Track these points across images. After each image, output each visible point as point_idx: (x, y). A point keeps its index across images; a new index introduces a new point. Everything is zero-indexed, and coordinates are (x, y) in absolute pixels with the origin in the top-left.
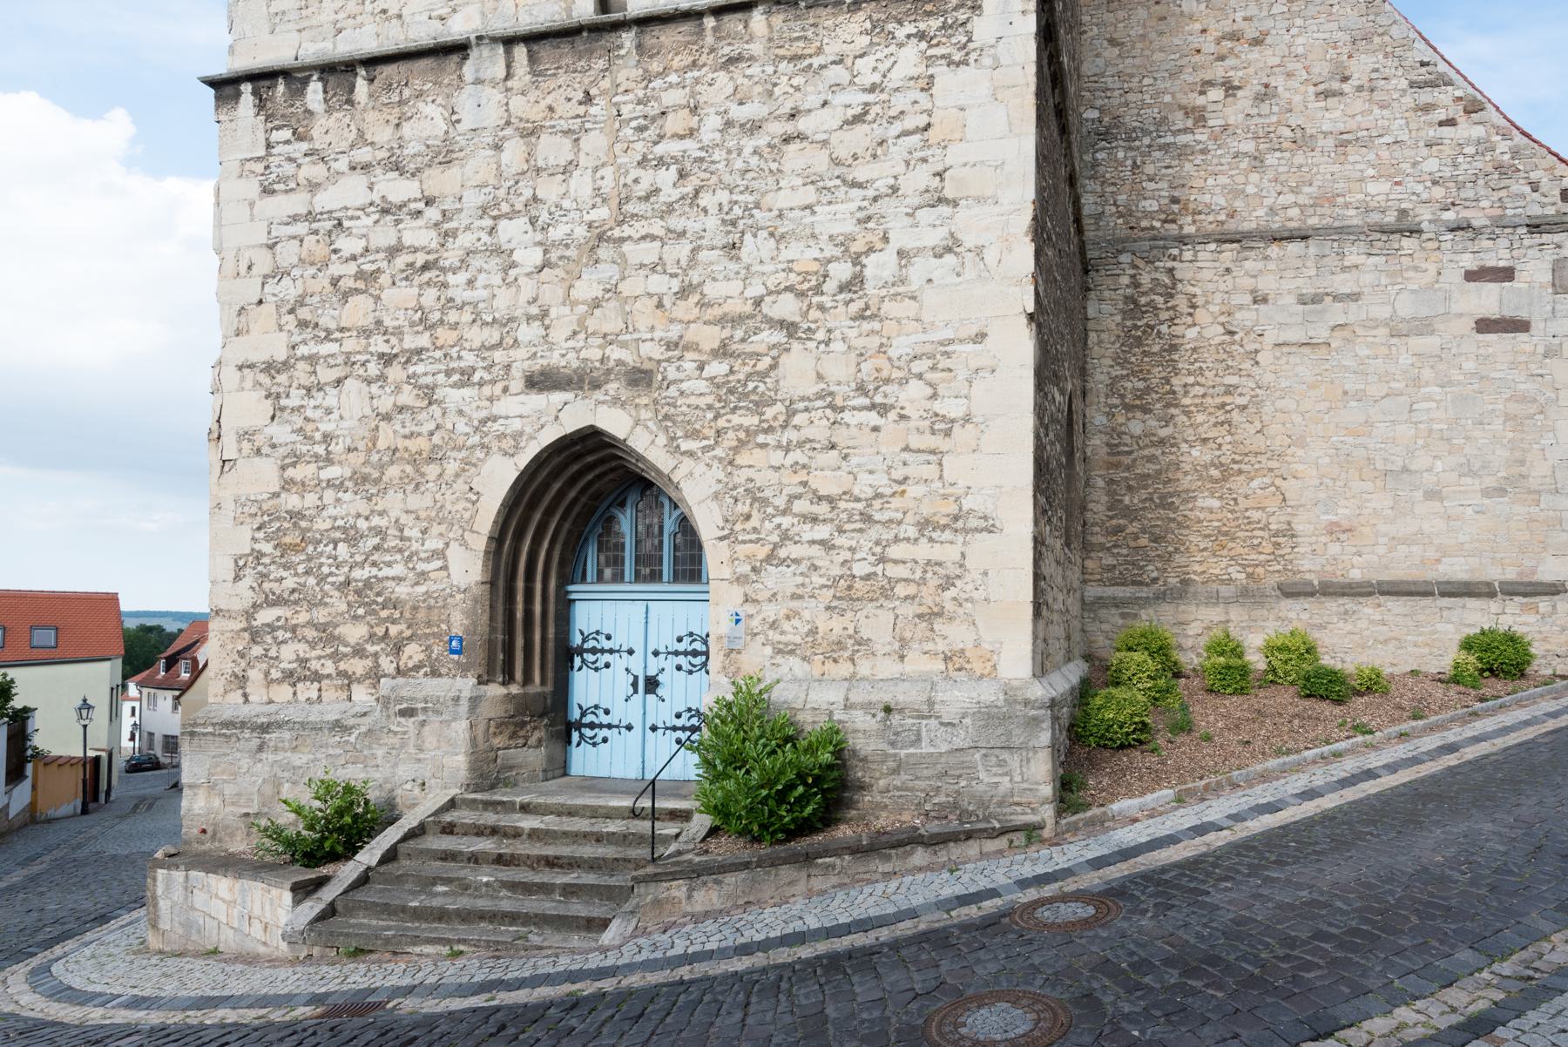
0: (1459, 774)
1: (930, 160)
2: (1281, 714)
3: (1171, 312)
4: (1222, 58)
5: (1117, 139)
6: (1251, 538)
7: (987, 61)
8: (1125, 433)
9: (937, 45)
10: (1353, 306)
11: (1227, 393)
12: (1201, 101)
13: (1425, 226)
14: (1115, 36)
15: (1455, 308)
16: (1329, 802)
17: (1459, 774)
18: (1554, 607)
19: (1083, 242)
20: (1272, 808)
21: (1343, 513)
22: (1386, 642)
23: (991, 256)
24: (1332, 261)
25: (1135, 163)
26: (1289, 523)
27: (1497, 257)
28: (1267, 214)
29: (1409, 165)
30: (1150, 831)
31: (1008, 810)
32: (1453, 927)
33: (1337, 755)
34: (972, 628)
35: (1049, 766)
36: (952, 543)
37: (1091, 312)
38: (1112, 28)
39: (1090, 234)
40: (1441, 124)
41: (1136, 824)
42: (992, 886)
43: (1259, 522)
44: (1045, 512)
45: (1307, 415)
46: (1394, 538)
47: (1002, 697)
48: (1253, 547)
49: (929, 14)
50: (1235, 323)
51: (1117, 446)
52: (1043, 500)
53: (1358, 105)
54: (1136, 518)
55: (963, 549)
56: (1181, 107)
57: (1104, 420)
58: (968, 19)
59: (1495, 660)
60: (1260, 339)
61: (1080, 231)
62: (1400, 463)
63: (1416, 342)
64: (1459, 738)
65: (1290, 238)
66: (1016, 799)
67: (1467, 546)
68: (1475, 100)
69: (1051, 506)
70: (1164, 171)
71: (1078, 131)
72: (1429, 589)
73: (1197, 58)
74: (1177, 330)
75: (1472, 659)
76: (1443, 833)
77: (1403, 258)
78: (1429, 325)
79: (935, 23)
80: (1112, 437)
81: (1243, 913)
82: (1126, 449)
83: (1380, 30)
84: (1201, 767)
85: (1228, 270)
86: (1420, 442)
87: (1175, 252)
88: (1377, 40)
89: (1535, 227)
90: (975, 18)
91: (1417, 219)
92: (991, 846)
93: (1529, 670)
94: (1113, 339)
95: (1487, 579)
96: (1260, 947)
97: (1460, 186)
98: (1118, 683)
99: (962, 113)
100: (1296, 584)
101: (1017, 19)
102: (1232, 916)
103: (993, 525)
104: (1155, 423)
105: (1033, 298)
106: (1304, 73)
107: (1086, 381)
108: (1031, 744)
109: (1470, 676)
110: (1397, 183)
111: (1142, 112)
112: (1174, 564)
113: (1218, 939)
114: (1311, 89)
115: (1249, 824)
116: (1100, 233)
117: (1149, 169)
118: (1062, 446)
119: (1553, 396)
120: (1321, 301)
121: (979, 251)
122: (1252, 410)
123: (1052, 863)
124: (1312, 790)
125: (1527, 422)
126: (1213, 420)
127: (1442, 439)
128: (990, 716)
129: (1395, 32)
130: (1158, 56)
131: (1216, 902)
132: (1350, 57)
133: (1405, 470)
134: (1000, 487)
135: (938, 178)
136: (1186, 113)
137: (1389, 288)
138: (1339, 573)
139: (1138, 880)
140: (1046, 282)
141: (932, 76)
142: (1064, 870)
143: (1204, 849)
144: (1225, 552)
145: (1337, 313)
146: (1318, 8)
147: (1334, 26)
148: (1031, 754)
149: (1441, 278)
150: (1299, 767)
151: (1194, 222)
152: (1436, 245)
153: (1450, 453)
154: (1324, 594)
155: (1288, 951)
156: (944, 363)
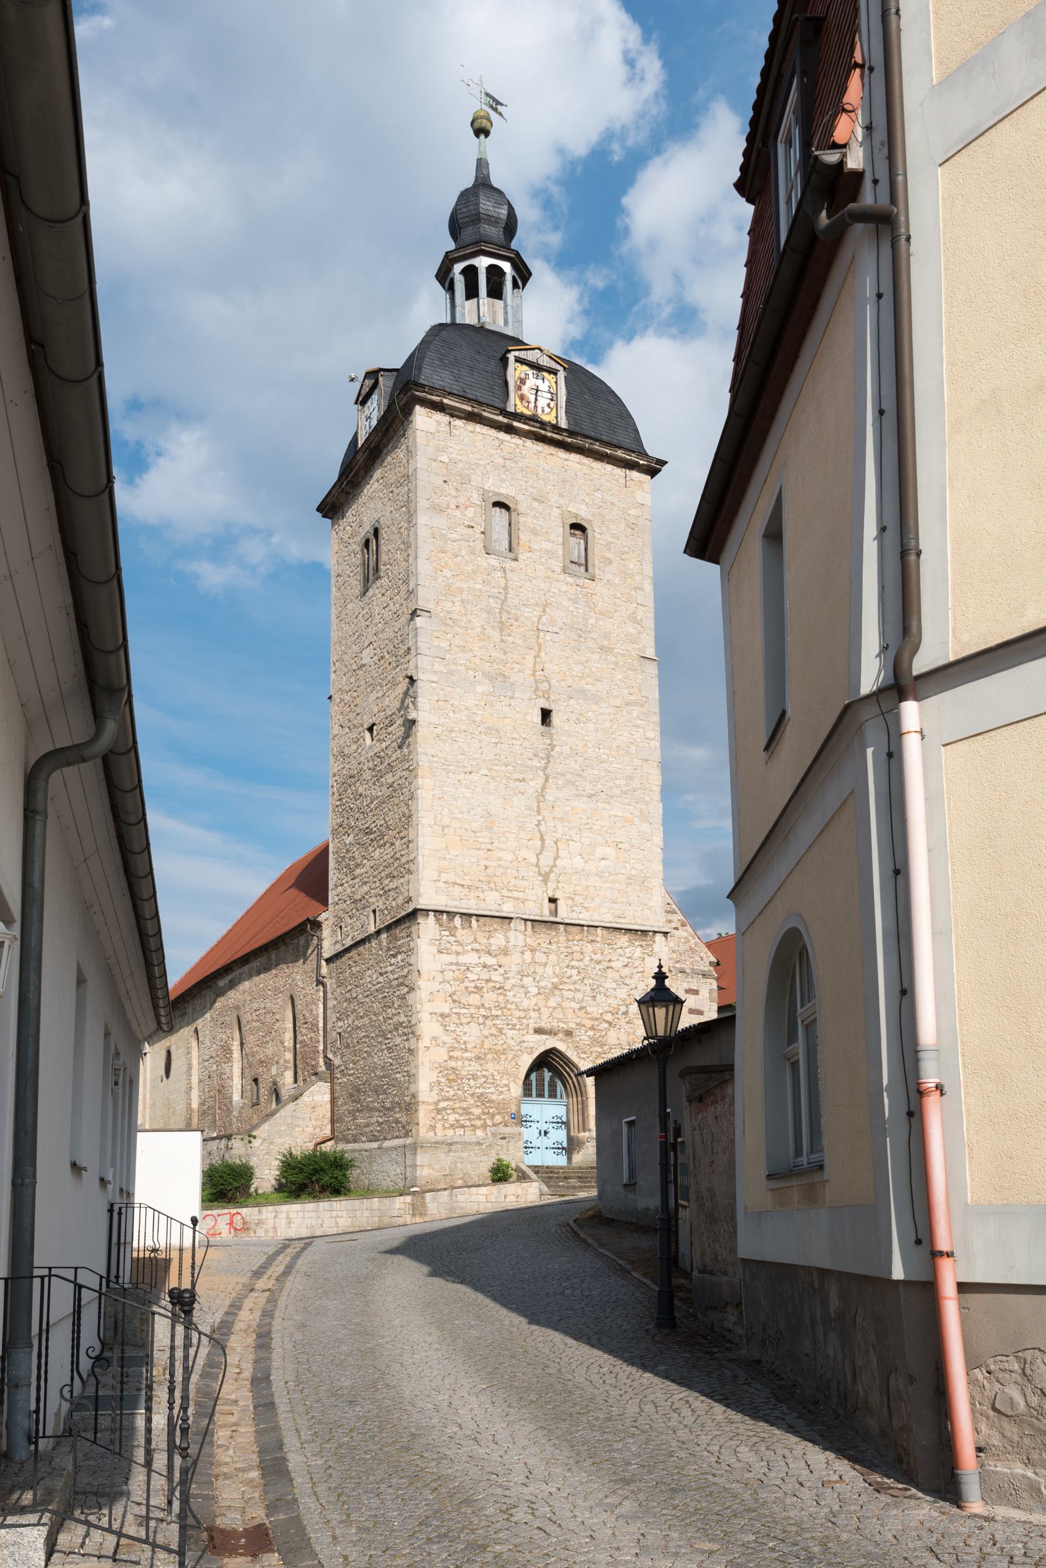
97: (681, 954)
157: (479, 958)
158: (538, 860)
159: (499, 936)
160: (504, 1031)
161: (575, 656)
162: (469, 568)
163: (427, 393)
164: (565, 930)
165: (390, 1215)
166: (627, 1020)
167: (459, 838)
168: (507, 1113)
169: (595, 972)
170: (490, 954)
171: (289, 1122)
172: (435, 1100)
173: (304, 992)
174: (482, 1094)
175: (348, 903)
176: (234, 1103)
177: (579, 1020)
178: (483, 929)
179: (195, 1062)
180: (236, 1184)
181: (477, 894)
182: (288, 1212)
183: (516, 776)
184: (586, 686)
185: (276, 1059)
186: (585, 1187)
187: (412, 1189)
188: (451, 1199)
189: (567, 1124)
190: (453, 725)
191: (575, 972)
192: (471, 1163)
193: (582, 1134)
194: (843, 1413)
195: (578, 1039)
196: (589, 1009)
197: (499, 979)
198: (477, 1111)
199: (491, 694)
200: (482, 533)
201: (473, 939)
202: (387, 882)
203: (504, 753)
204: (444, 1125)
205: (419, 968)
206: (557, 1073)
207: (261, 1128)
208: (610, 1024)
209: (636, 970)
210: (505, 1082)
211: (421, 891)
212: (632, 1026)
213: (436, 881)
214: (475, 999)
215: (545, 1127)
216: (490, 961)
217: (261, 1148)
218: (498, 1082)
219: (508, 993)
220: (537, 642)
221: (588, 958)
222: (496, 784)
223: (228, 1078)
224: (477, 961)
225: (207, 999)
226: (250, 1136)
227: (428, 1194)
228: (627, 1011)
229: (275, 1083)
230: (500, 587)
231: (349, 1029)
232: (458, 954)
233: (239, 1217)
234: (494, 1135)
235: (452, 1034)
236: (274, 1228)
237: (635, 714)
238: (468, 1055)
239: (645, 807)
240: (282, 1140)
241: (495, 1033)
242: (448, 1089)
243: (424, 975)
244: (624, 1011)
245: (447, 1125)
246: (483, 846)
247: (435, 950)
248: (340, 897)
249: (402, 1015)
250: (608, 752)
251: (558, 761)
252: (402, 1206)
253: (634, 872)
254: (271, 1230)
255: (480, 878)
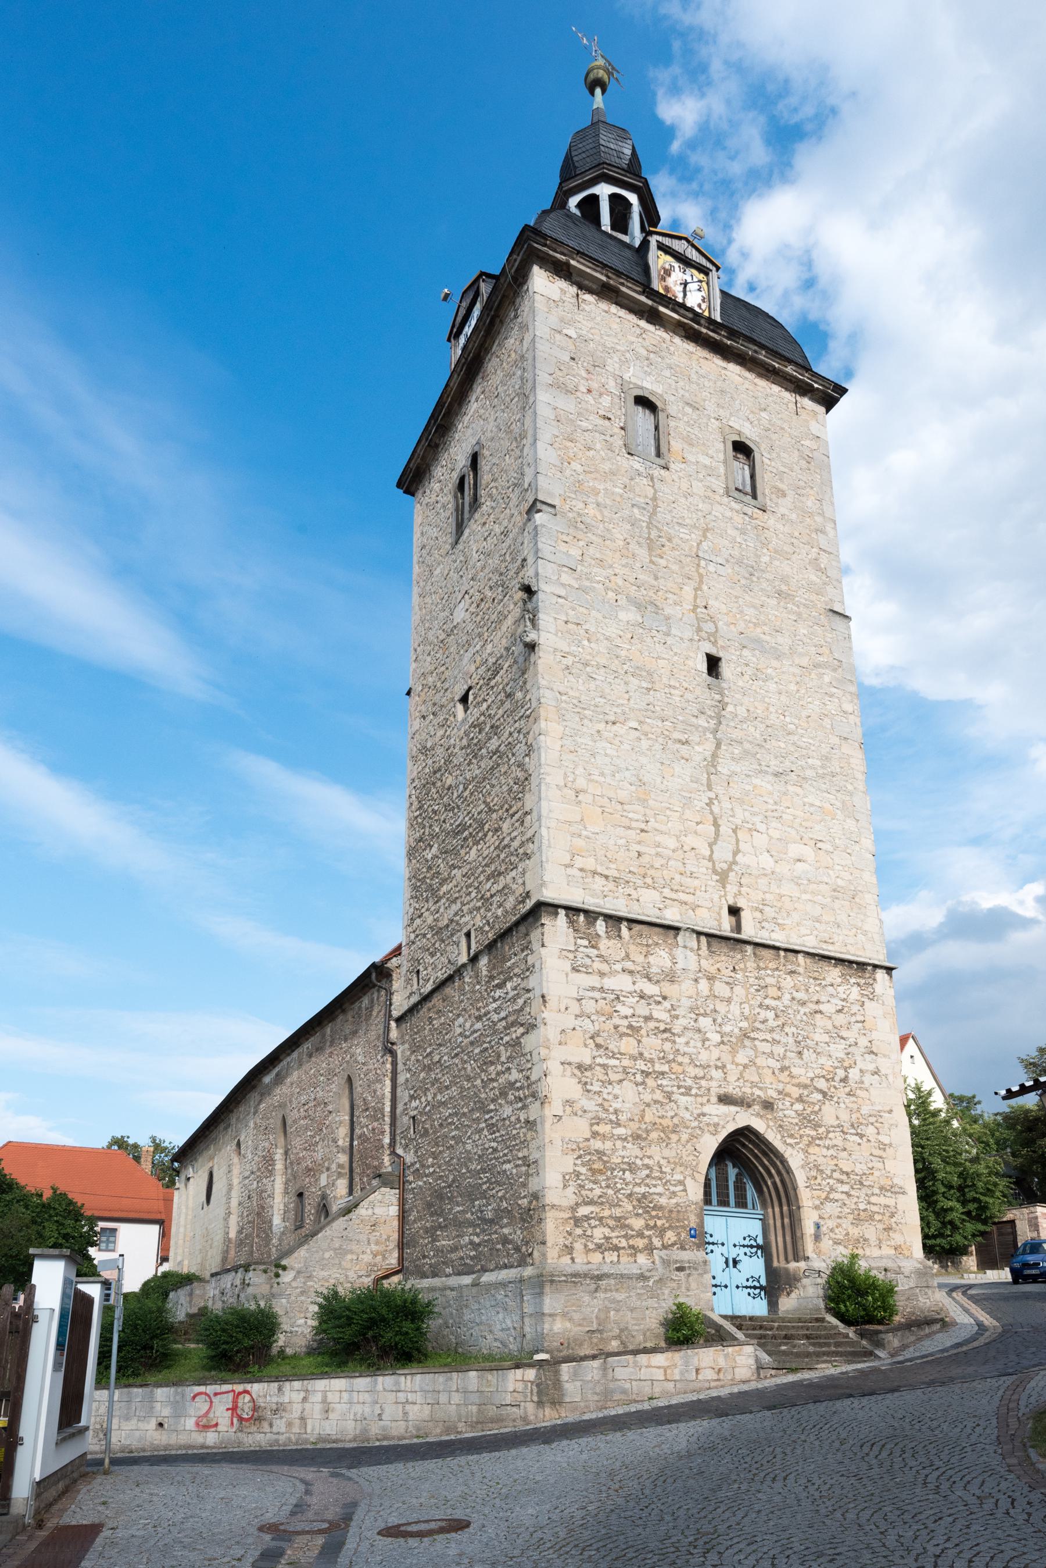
157: (634, 983)
158: (712, 852)
159: (662, 953)
160: (674, 1097)
161: (747, 597)
162: (607, 466)
163: (549, 247)
164: (754, 954)
165: (498, 1402)
166: (847, 1089)
167: (600, 810)
168: (683, 1227)
169: (798, 1017)
170: (650, 980)
171: (337, 1246)
172: (572, 1203)
173: (365, 1068)
174: (644, 1196)
175: (429, 936)
176: (274, 1228)
177: (781, 1087)
178: (638, 941)
179: (236, 1181)
180: (247, 1343)
181: (628, 891)
182: (325, 1393)
183: (676, 735)
184: (762, 636)
185: (326, 1164)
186: (824, 1354)
187: (537, 1357)
188: (605, 1375)
189: (765, 1249)
190: (588, 657)
191: (770, 1015)
192: (632, 1310)
193: (793, 1265)
195: (781, 1114)
196: (795, 1071)
197: (665, 1016)
198: (638, 1223)
199: (641, 625)
200: (622, 428)
201: (623, 954)
202: (489, 884)
203: (660, 703)
204: (586, 1246)
205: (545, 992)
206: (747, 1168)
207: (296, 1254)
208: (824, 1094)
209: (853, 1019)
210: (678, 1177)
211: (545, 878)
212: (853, 1099)
213: (567, 866)
214: (628, 1045)
215: (733, 1253)
216: (650, 989)
217: (294, 1284)
218: (669, 1177)
219: (677, 1039)
220: (697, 571)
221: (787, 997)
222: (650, 742)
223: (269, 1196)
224: (631, 988)
225: (252, 1103)
226: (278, 1266)
227: (565, 1367)
228: (847, 1077)
229: (324, 1197)
230: (646, 497)
231: (428, 1108)
232: (602, 974)
233: (247, 1398)
234: (666, 1263)
235: (596, 1097)
236: (302, 1419)
237: (827, 679)
238: (621, 1131)
239: (848, 798)
240: (325, 1274)
241: (660, 1098)
242: (591, 1185)
243: (552, 1003)
244: (843, 1076)
245: (591, 1246)
246: (634, 824)
247: (567, 966)
248: (417, 932)
249: (514, 1071)
250: (797, 721)
251: (732, 724)
252: (520, 1386)
253: (840, 882)
254: (297, 1422)
255: (632, 869)
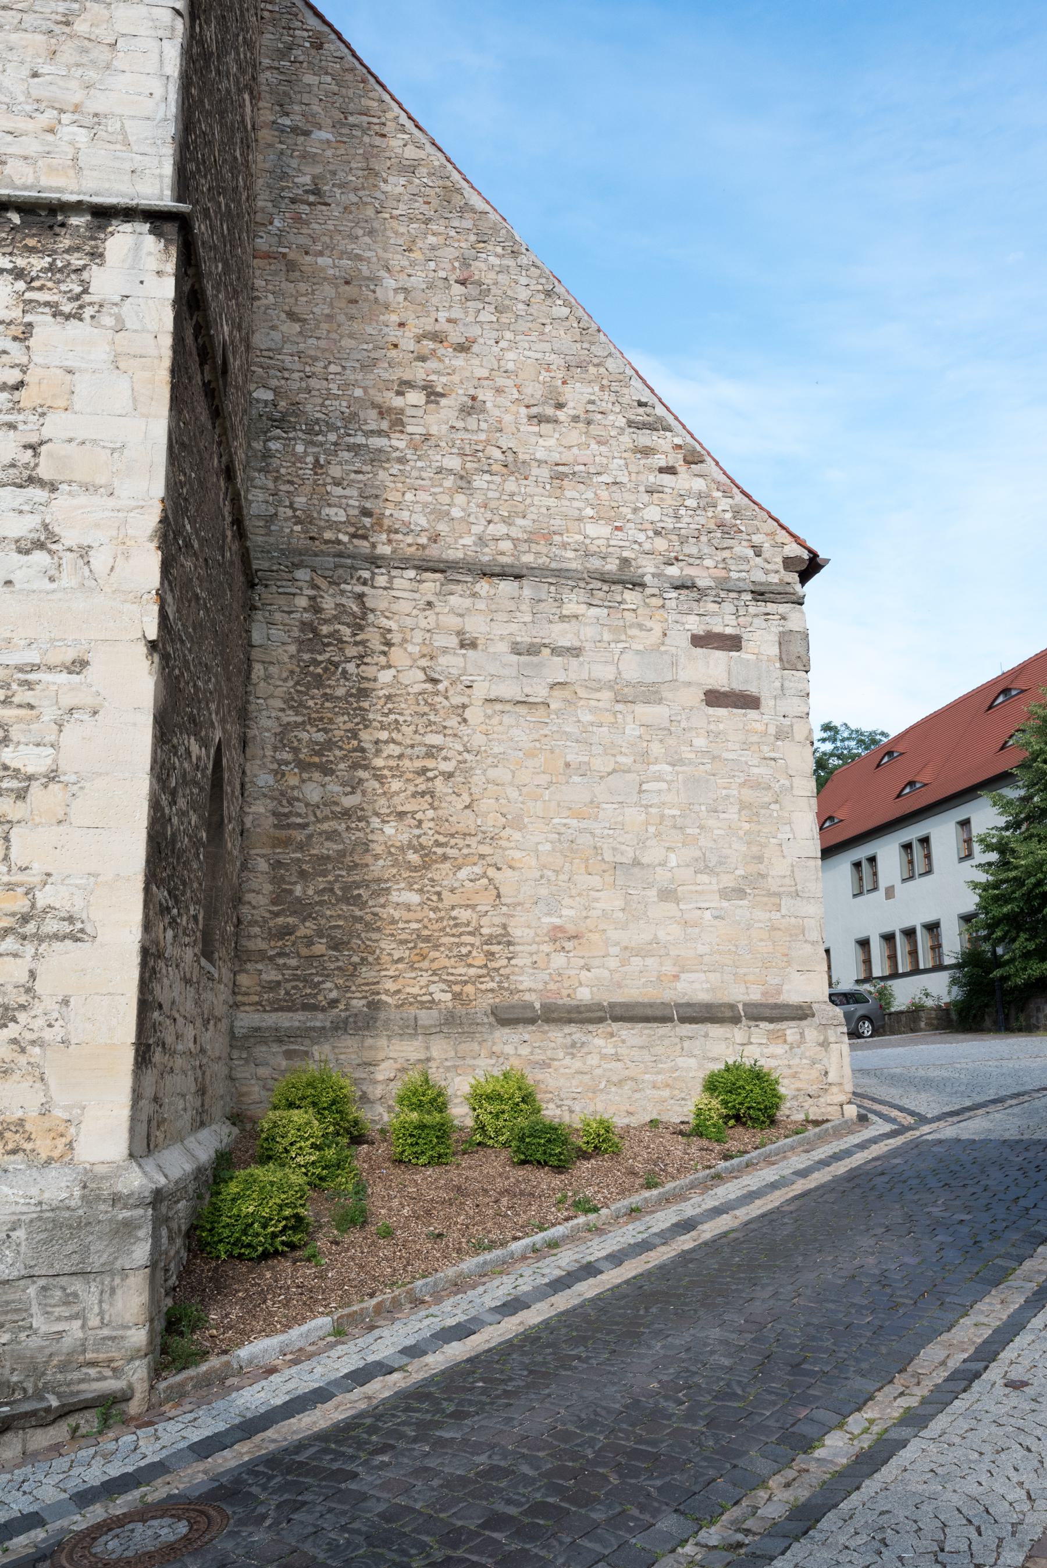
0: (692, 1261)
1: (21, 427)
2: (486, 1191)
3: (361, 648)
4: (423, 359)
5: (295, 430)
6: (459, 945)
7: (107, 320)
8: (298, 800)
9: (41, 288)
10: (574, 662)
11: (429, 755)
12: (398, 402)
13: (648, 579)
14: (295, 309)
15: (683, 676)
16: (534, 1316)
17: (692, 1261)
18: (802, 1034)
19: (247, 549)
20: (461, 1332)
21: (568, 914)
22: (620, 1083)
23: (100, 561)
24: (548, 607)
25: (317, 461)
26: (505, 926)
27: (724, 623)
28: (475, 544)
29: (629, 510)
30: (290, 1385)
31: (76, 1375)
32: (658, 1483)
33: (553, 1245)
34: (38, 1085)
35: (144, 1298)
36: (15, 955)
37: (257, 637)
38: (292, 300)
39: (257, 538)
40: (661, 470)
41: (272, 1378)
42: (32, 1509)
43: (468, 925)
44: (165, 910)
45: (525, 790)
46: (626, 948)
47: (77, 1192)
48: (461, 957)
49: (32, 250)
50: (438, 669)
51: (287, 815)
52: (161, 894)
53: (574, 435)
54: (310, 916)
55: (33, 966)
56: (374, 405)
57: (271, 780)
58: (85, 267)
59: (741, 1104)
60: (468, 691)
61: (241, 534)
62: (631, 855)
63: (643, 711)
64: (698, 1211)
65: (502, 575)
66: (90, 1356)
67: (706, 959)
68: (694, 451)
69: (177, 901)
70: (353, 476)
71: (245, 411)
72: (667, 1012)
73: (393, 353)
74: (369, 671)
75: (715, 1103)
76: (663, 1347)
77: (626, 613)
78: (656, 692)
79: (38, 263)
80: (280, 803)
81: (397, 1501)
82: (299, 820)
83: (596, 361)
84: (374, 1279)
85: (429, 604)
86: (652, 829)
87: (366, 574)
88: (592, 370)
89: (760, 594)
90: (94, 267)
91: (640, 571)
92: (41, 1439)
93: (780, 1115)
94: (285, 675)
95: (726, 999)
96: (413, 1551)
97: (683, 541)
98: (270, 1158)
99: (69, 377)
100: (513, 1007)
101: (151, 279)
102: (382, 1507)
103: (82, 931)
104: (337, 789)
105: (156, 621)
106: (515, 391)
107: (246, 726)
108: (118, 1265)
109: (714, 1125)
110: (617, 528)
111: (327, 402)
112: (359, 981)
113: (358, 1547)
114: (523, 411)
115: (429, 1359)
116: (272, 540)
117: (335, 471)
118: (200, 817)
119: (787, 783)
120: (537, 653)
121: (84, 552)
122: (459, 779)
123: (137, 1455)
124: (516, 1299)
125: (763, 811)
126: (411, 788)
127: (675, 827)
128: (57, 1224)
129: (610, 363)
130: (347, 343)
131: (365, 1489)
132: (565, 383)
133: (636, 863)
134: (96, 875)
135: (30, 452)
136: (381, 413)
137: (613, 645)
138: (565, 992)
139: (261, 1468)
140: (179, 601)
141: (30, 325)
142: (153, 1465)
143: (363, 1406)
144: (425, 964)
145: (555, 669)
146: (529, 325)
147: (547, 346)
148: (117, 1280)
149: (667, 640)
150: (503, 1267)
151: (390, 541)
152: (660, 602)
153: (684, 844)
154: (548, 1021)
155: (450, 1552)
156: (22, 696)
194: (420, 1162)
